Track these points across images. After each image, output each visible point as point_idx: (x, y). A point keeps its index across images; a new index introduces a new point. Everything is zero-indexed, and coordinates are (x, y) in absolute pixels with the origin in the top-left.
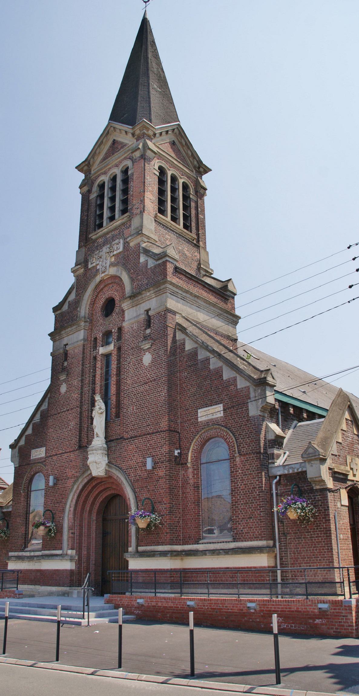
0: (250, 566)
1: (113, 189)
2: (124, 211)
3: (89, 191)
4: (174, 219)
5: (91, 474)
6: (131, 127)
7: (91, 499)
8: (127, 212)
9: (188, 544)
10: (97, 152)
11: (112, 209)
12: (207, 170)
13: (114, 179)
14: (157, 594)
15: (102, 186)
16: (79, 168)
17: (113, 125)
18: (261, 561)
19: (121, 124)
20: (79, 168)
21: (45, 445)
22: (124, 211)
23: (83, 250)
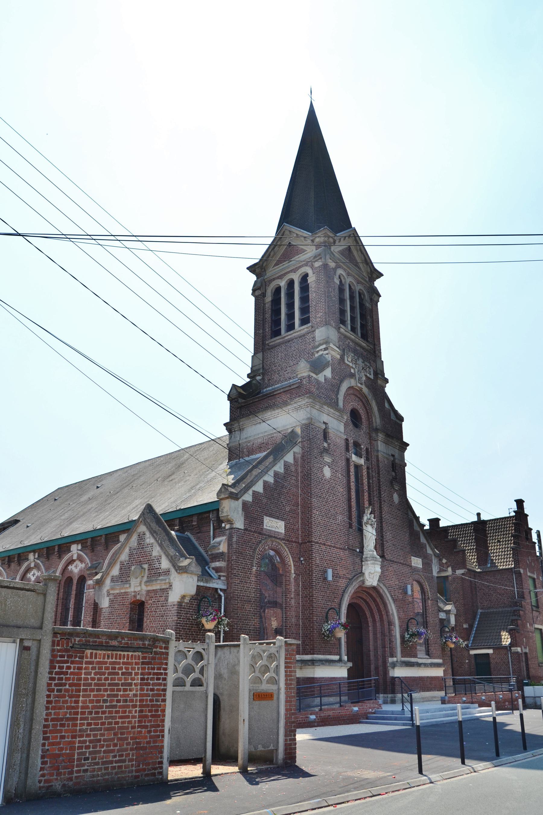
0: (131, 807)
1: (290, 295)
2: (305, 321)
3: (264, 295)
4: (353, 329)
5: (363, 582)
6: (310, 234)
7: (369, 600)
8: (309, 322)
9: (238, 685)
10: (272, 254)
11: (291, 316)
12: (380, 275)
13: (291, 283)
14: (322, 707)
15: (278, 290)
16: (252, 269)
17: (288, 228)
18: (439, 672)
19: (299, 229)
20: (252, 269)
21: (423, 568)
22: (305, 321)
23: (260, 355)
